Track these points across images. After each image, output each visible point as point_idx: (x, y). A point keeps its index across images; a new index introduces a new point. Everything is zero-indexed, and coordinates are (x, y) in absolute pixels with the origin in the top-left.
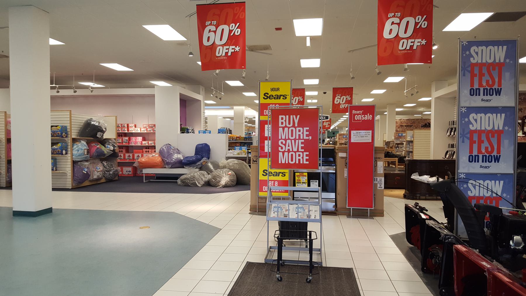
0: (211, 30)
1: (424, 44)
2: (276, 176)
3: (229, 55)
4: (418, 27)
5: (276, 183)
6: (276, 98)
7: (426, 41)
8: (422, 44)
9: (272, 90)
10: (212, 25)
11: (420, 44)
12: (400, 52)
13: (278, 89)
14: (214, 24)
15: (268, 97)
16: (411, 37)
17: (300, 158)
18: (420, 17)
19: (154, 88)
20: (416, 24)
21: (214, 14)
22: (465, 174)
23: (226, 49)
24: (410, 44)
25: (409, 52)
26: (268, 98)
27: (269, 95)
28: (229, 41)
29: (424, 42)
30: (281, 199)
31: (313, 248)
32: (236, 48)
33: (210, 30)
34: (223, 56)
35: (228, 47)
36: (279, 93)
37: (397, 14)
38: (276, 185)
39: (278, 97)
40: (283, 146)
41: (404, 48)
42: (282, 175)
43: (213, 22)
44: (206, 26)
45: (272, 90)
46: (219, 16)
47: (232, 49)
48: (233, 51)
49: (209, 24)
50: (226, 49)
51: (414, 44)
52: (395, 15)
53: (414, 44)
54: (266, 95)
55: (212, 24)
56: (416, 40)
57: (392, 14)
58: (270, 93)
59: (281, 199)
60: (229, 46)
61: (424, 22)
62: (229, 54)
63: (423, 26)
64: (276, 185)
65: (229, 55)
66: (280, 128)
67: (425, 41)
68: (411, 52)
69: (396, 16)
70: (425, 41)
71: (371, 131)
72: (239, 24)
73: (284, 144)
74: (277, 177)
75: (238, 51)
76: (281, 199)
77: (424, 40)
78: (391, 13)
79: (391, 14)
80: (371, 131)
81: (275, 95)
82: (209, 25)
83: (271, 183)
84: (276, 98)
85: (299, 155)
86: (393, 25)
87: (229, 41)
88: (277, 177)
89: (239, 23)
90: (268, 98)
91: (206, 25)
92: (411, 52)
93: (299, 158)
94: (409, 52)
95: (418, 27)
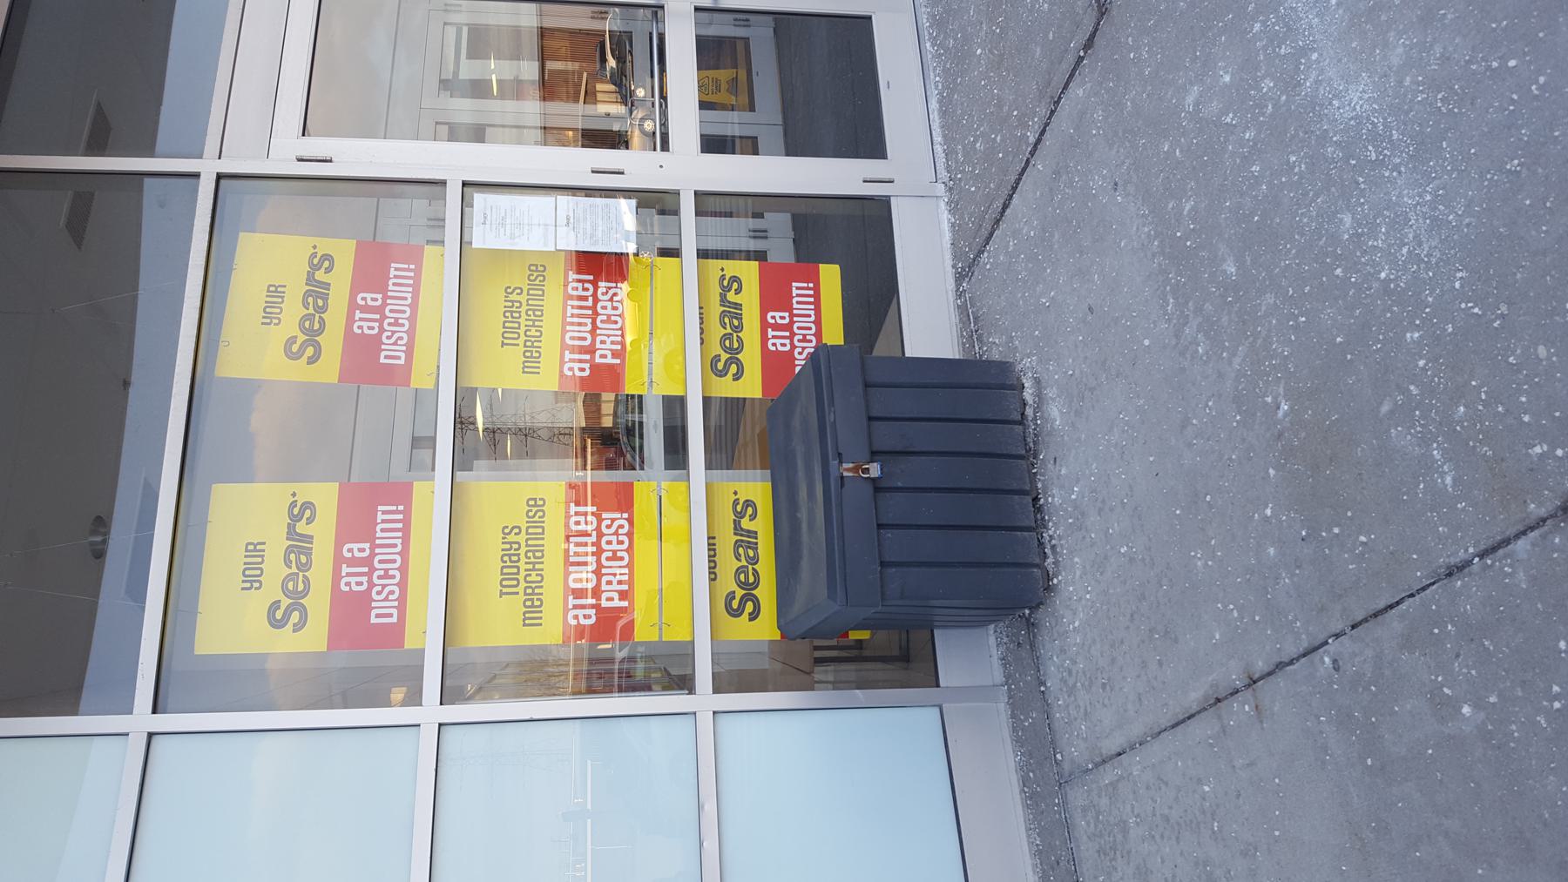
2: (740, 319)
5: (350, 550)
6: (751, 553)
9: (252, 580)
13: (255, 550)
15: (749, 597)
17: (608, 340)
19: (434, 480)
22: (1478, 556)
26: (754, 592)
27: (734, 587)
30: (688, 206)
31: (770, 483)
36: (277, 546)
38: (362, 550)
39: (299, 545)
40: (616, 524)
42: (747, 517)
45: (252, 580)
54: (735, 604)
58: (272, 589)
59: (685, 683)
64: (362, 550)
74: (760, 541)
76: (688, 206)
81: (288, 563)
84: (751, 553)
85: (609, 583)
88: (285, 536)
90: (754, 592)
93: (615, 583)
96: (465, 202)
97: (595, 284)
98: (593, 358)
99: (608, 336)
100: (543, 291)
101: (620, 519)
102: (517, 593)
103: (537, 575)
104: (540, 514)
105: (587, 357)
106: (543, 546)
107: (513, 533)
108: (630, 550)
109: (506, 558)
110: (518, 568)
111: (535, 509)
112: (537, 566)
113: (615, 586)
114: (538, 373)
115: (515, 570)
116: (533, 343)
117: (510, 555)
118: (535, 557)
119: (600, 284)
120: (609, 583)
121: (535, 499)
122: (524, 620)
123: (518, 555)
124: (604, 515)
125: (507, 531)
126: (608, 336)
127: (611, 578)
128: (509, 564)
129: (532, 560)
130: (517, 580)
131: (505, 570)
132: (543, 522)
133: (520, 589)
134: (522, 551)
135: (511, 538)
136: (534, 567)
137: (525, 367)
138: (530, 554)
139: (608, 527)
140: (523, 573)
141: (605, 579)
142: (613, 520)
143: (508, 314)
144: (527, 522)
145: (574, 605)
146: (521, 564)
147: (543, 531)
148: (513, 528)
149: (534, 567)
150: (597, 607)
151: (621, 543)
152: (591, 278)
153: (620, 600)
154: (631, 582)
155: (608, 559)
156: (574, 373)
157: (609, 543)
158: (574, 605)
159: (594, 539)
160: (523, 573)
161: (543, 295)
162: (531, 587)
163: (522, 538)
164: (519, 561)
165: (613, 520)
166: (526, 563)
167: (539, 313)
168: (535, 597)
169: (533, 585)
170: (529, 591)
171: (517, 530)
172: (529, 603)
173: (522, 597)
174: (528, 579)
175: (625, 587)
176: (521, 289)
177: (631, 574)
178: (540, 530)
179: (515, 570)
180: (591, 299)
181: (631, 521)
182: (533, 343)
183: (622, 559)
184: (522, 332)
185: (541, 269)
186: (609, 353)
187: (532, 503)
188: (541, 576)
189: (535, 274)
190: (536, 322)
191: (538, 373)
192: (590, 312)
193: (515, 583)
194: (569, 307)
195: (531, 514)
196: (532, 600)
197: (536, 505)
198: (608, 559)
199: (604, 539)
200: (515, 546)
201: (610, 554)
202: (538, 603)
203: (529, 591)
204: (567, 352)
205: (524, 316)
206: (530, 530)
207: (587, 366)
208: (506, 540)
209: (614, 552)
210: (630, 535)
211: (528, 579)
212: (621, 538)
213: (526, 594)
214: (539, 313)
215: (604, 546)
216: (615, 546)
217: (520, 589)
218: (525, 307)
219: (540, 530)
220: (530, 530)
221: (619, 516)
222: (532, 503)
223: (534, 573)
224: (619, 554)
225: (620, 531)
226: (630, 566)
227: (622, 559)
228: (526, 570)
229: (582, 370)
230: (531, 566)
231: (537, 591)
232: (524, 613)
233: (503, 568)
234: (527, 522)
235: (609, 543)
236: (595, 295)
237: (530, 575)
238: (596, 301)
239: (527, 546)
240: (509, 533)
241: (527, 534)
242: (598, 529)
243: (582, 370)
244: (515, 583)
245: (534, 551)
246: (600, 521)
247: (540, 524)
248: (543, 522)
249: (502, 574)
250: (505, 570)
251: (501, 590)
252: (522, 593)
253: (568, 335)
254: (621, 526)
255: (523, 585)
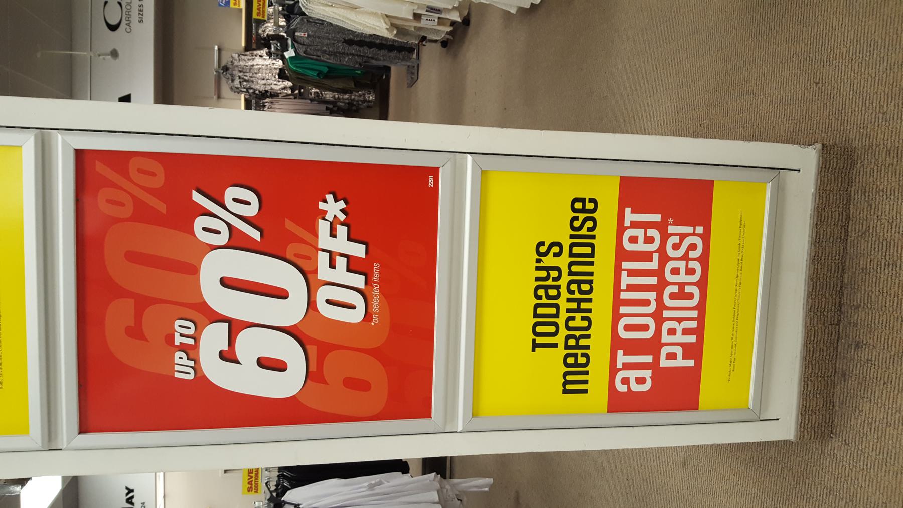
0: (226, 348)
1: (342, 204)
3: (362, 255)
4: (256, 235)
7: (329, 197)
8: (342, 217)
10: (196, 346)
11: (342, 224)
12: (375, 319)
14: (191, 332)
16: (305, 268)
17: (679, 328)
18: (201, 222)
20: (237, 242)
21: (136, 332)
23: (332, 265)
24: (340, 274)
25: (376, 277)
28: (291, 251)
29: (333, 208)
32: (330, 217)
33: (223, 355)
34: (366, 283)
35: (323, 259)
37: (181, 335)
40: (688, 241)
41: (357, 300)
43: (178, 340)
44: (201, 379)
46: (143, 303)
47: (333, 234)
48: (342, 231)
49: (192, 363)
50: (332, 265)
51: (342, 255)
52: (183, 348)
53: (342, 255)
55: (192, 341)
56: (320, 246)
57: (177, 360)
60: (318, 249)
61: (228, 202)
62: (359, 250)
63: (252, 210)
65: (362, 255)
66: (621, 293)
67: (325, 201)
68: (377, 266)
69: (192, 341)
70: (325, 201)
71: (648, 235)
72: (199, 191)
73: (681, 240)
75: (346, 202)
77: (322, 205)
78: (173, 364)
79: (177, 368)
80: (648, 235)
82: (196, 361)
83: (632, 374)
85: (672, 332)
86: (239, 356)
87: (291, 251)
89: (194, 192)
91: (191, 377)
92: (377, 266)
93: (679, 332)
94: (376, 277)
95: (256, 235)
96: (483, 175)
97: (662, 227)
98: (657, 358)
99: (680, 320)
100: (592, 246)
101: (692, 235)
102: (555, 345)
103: (583, 319)
104: (590, 224)
105: (648, 359)
106: (591, 274)
107: (551, 254)
108: (702, 284)
109: (541, 292)
110: (557, 307)
111: (582, 216)
112: (584, 306)
113: (679, 338)
114: (586, 391)
115: (553, 311)
116: (578, 340)
117: (547, 288)
118: (581, 292)
119: (672, 229)
120: (672, 332)
121: (583, 200)
122: (564, 385)
123: (558, 288)
124: (672, 229)
125: (543, 249)
126: (680, 320)
127: (673, 325)
128: (544, 301)
129: (577, 295)
130: (556, 325)
131: (540, 311)
132: (594, 237)
133: (560, 339)
134: (564, 282)
135: (549, 261)
136: (579, 306)
137: (566, 382)
138: (574, 287)
139: (676, 247)
140: (564, 315)
141: (666, 326)
142: (683, 236)
143: (541, 292)
144: (572, 237)
145: (631, 222)
146: (562, 302)
147: (593, 250)
148: (553, 244)
149: (579, 306)
150: (654, 366)
151: (690, 272)
152: (657, 218)
153: (685, 357)
154: (699, 332)
155: (673, 296)
156: (629, 387)
157: (675, 271)
158: (631, 222)
159: (654, 265)
160: (564, 315)
161: (592, 255)
162: (573, 337)
163: (563, 262)
164: (558, 297)
165: (683, 236)
166: (569, 300)
167: (586, 287)
168: (580, 351)
169: (578, 334)
170: (572, 342)
171: (556, 249)
172: (571, 360)
173: (561, 351)
174: (572, 324)
175: (692, 339)
176: (560, 245)
177: (701, 319)
178: (588, 250)
179: (553, 311)
180: (656, 256)
181: (706, 238)
182: (578, 340)
183: (690, 296)
184: (561, 321)
185: (589, 206)
186: (679, 350)
187: (579, 205)
188: (588, 319)
189: (582, 216)
190: (581, 306)
191: (586, 391)
192: (653, 281)
193: (552, 329)
194: (624, 274)
195: (577, 224)
196: (575, 355)
197: (584, 210)
198: (673, 296)
199: (670, 265)
200: (554, 274)
201: (675, 289)
202: (582, 360)
203: (572, 342)
204: (628, 210)
205: (565, 295)
206: (576, 250)
207: (647, 374)
208: (541, 264)
209: (682, 286)
210: (704, 260)
211: (572, 324)
212: (692, 264)
213: (567, 347)
214: (586, 287)
215: (669, 277)
216: (682, 278)
217: (560, 339)
218: (565, 279)
219: (588, 250)
220: (576, 250)
221: (689, 229)
222: (579, 205)
223: (578, 316)
224: (688, 289)
225: (692, 254)
226: (701, 307)
227: (690, 296)
228: (568, 311)
229: (640, 381)
230: (574, 306)
231: (582, 342)
232: (565, 374)
233: (537, 306)
234: (572, 237)
235: (675, 271)
236: (662, 250)
237: (573, 319)
238: (664, 259)
239: (571, 273)
240: (546, 254)
241: (571, 255)
242: (662, 250)
243: (640, 381)
244: (552, 329)
245: (579, 283)
246: (665, 236)
247: (588, 240)
248: (594, 237)
249: (536, 315)
250: (540, 311)
251: (534, 340)
252: (562, 344)
253: (623, 322)
254: (693, 247)
255: (564, 332)
